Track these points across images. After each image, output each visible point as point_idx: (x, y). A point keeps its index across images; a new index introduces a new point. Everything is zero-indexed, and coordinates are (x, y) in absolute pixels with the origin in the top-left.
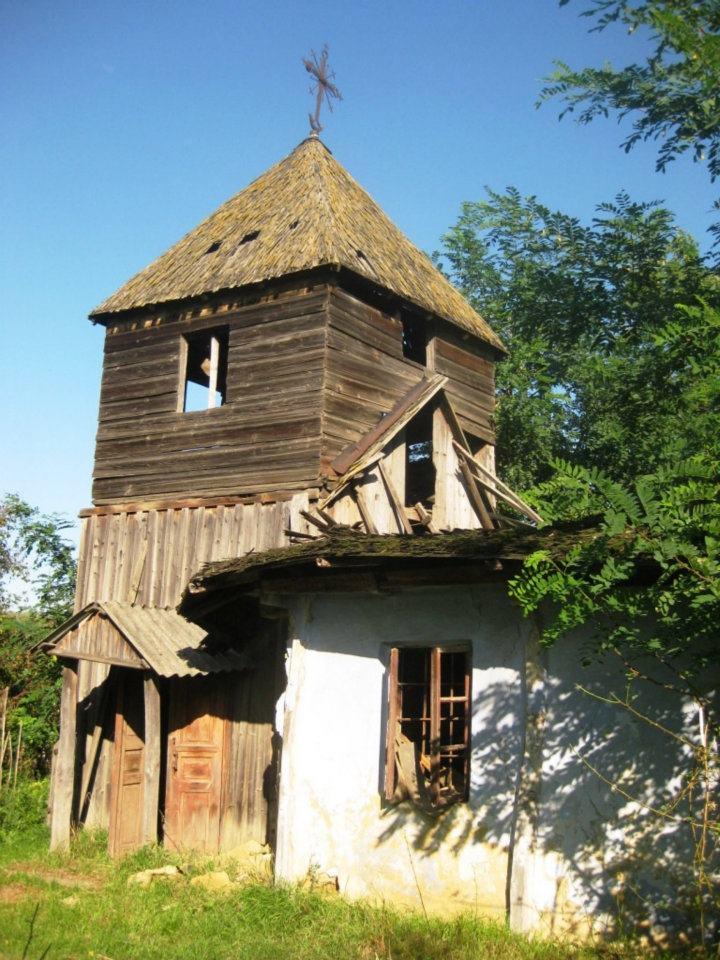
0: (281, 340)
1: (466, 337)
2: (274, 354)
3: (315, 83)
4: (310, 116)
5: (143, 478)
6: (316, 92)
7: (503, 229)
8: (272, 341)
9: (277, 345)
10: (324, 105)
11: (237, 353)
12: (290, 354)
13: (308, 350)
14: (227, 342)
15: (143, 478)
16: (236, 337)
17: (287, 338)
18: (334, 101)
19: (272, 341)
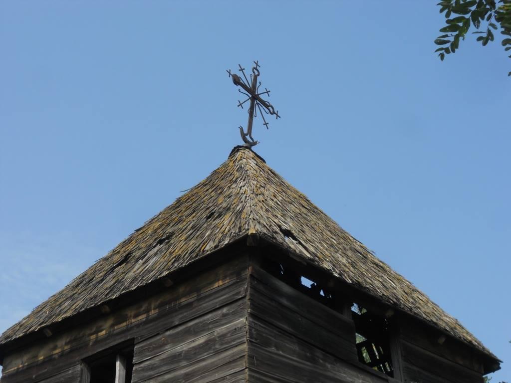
0: (193, 345)
1: (442, 340)
2: (184, 363)
3: (245, 97)
4: (242, 129)
5: (144, 271)
6: (248, 105)
7: (240, 205)
8: (183, 347)
9: (187, 352)
10: (257, 121)
11: (144, 370)
12: (204, 360)
13: (226, 350)
14: (132, 359)
15: (144, 271)
16: (141, 352)
17: (201, 340)
18: (270, 118)
19: (183, 347)
